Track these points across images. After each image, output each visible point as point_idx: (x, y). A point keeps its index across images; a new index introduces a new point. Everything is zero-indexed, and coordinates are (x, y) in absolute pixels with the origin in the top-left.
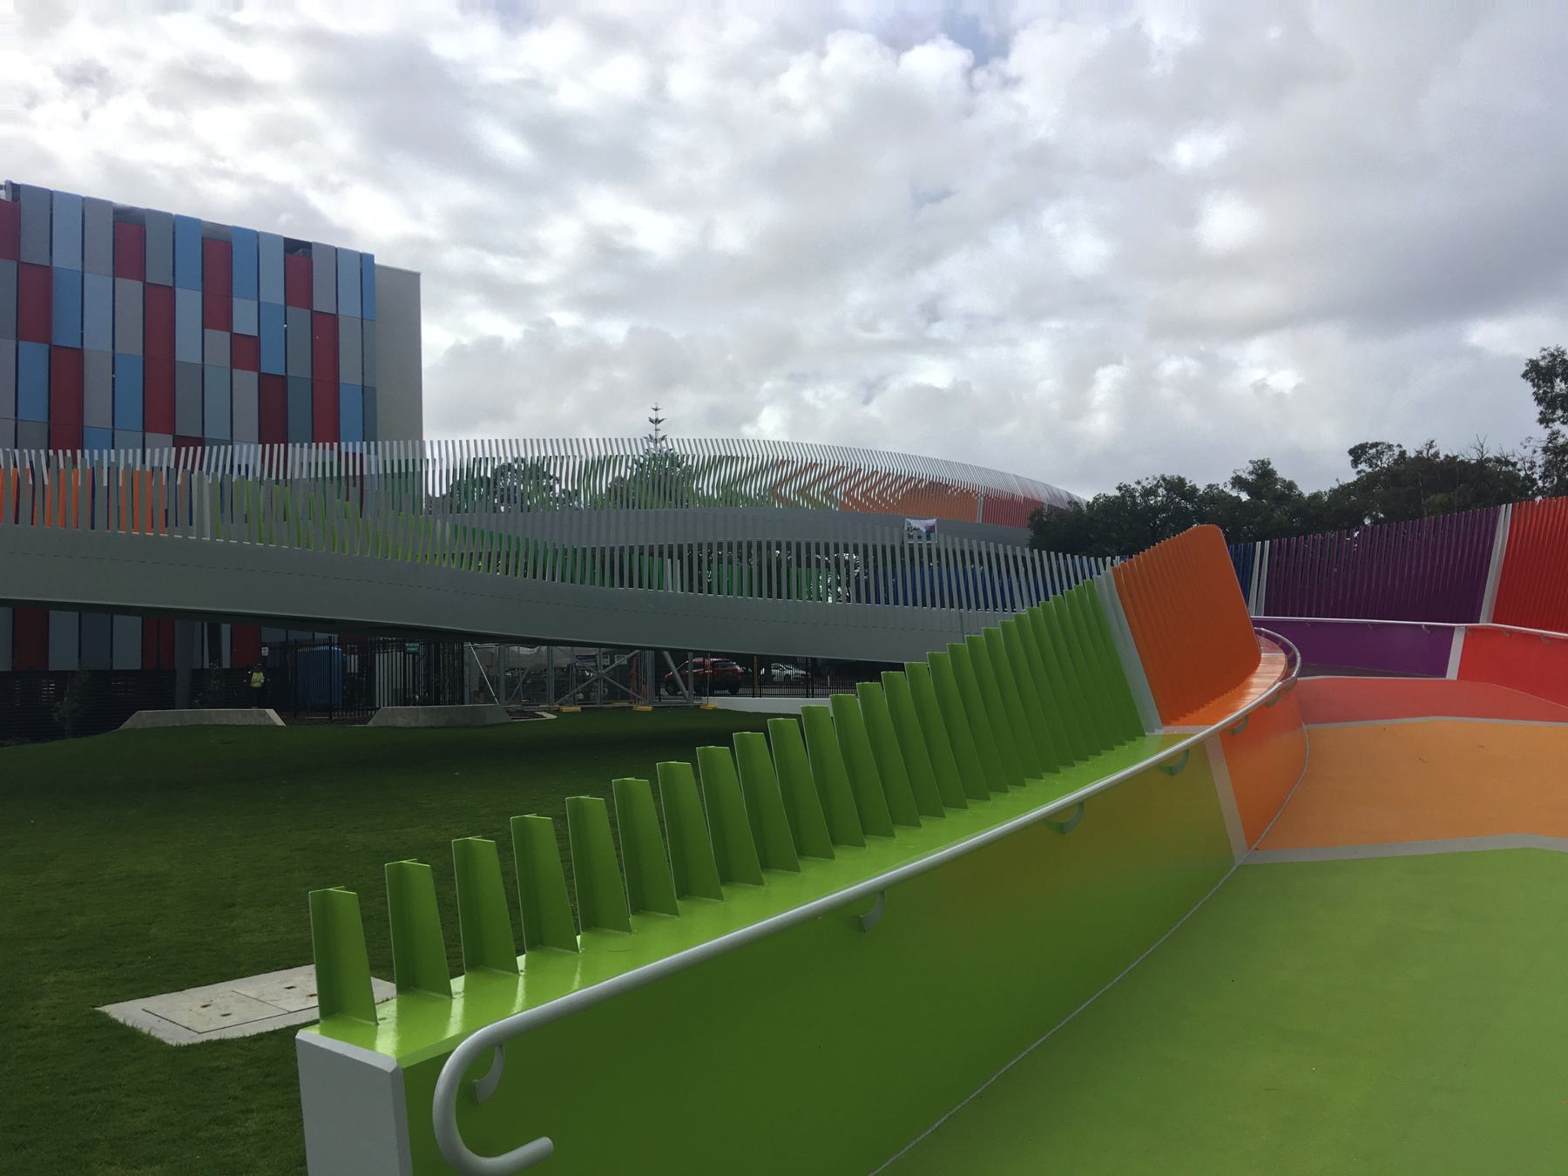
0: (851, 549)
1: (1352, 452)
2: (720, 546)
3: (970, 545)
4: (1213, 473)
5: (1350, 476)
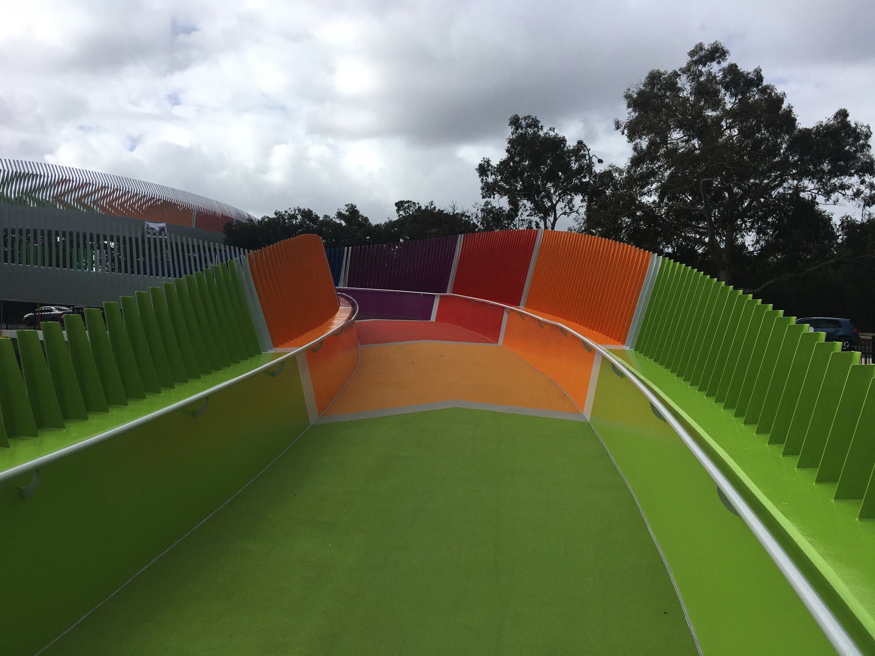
0: (108, 238)
1: (396, 204)
2: (13, 231)
3: (182, 239)
4: (327, 209)
5: (395, 217)
